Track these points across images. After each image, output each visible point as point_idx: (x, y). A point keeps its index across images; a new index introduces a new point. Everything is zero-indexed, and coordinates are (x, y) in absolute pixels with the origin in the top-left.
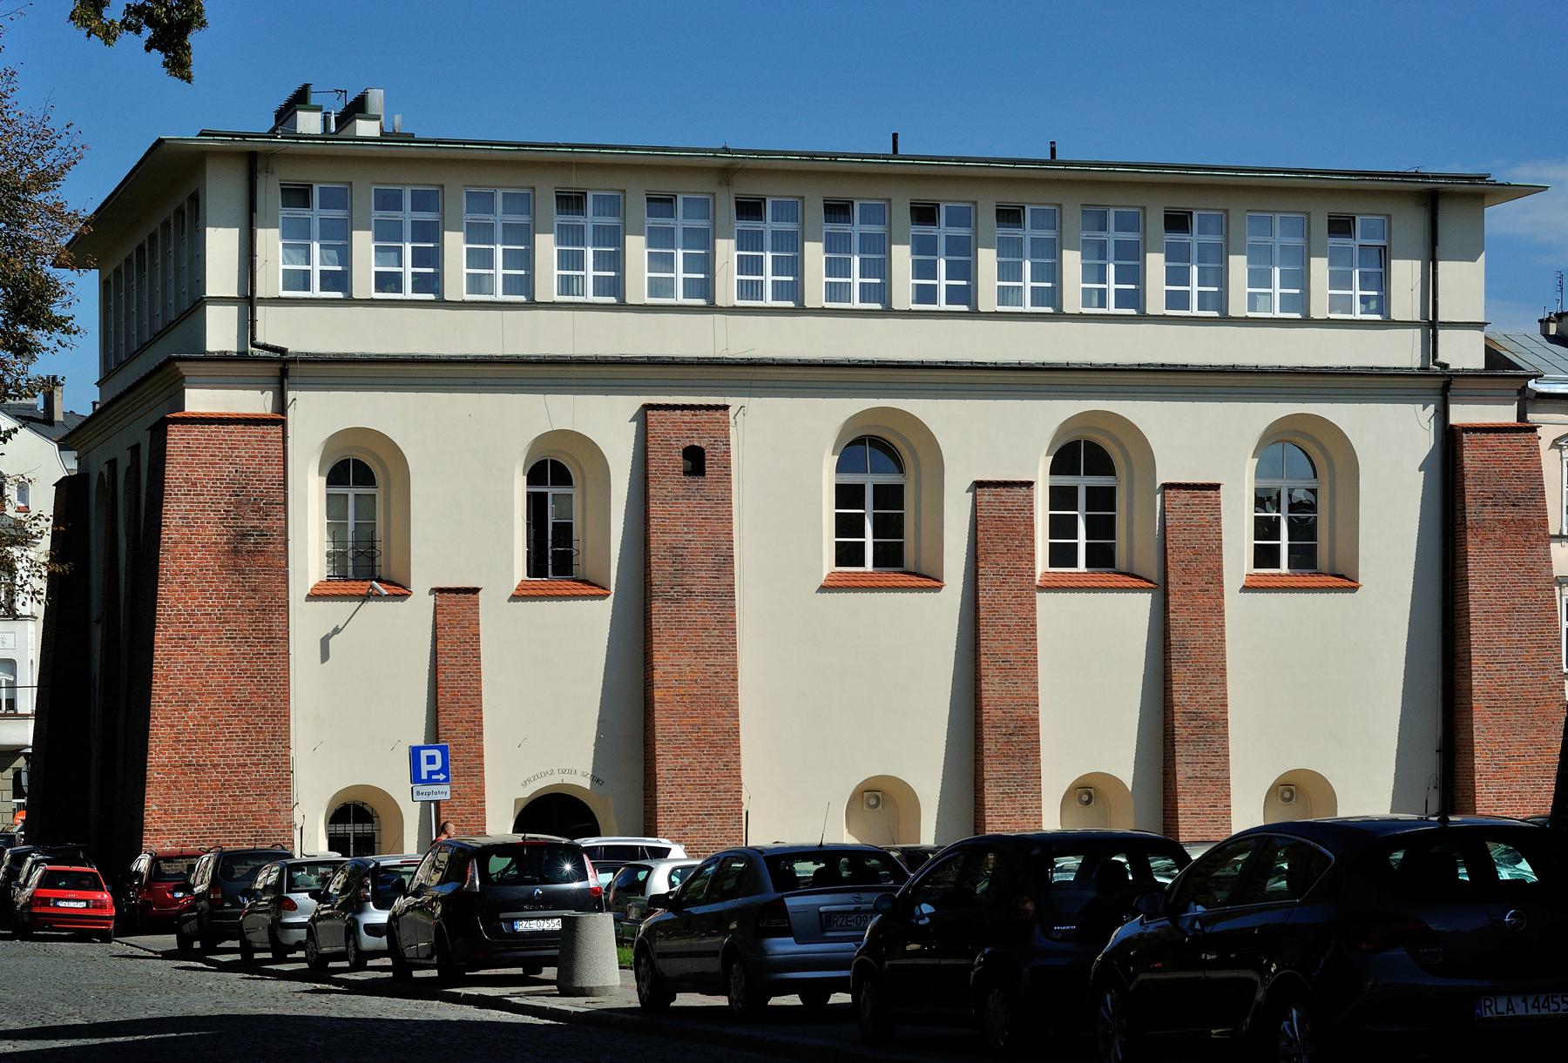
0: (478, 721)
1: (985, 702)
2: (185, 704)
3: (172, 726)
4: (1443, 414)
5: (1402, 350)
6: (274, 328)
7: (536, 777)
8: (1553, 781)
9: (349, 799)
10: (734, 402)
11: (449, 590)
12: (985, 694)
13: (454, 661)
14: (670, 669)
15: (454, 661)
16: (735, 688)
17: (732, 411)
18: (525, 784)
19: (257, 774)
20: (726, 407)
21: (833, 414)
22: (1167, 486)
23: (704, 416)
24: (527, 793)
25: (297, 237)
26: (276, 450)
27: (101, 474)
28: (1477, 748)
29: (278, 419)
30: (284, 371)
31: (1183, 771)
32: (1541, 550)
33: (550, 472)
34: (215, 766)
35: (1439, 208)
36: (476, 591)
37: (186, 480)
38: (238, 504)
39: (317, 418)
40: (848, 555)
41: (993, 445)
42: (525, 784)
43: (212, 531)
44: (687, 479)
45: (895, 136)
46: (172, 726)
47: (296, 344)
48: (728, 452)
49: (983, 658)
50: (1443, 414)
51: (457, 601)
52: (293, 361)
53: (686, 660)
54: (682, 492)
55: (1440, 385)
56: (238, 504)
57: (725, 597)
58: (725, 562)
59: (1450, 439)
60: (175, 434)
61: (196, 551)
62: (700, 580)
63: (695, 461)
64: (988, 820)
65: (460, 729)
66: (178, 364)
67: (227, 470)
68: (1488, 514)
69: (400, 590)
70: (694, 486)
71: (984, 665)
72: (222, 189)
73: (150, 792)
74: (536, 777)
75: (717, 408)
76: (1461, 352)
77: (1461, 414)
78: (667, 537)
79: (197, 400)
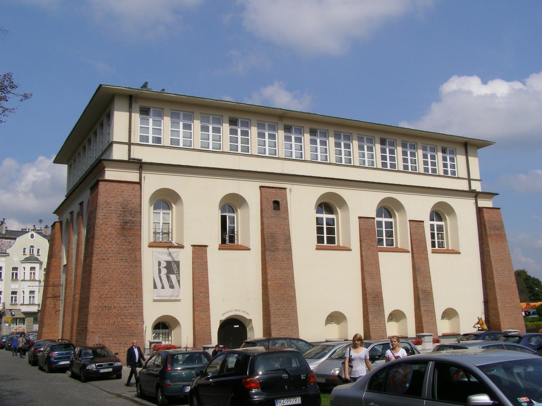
0: (207, 292)
1: (367, 287)
2: (104, 284)
3: (99, 292)
4: (476, 203)
5: (463, 185)
6: (138, 153)
8: (500, 318)
9: (161, 321)
11: (197, 246)
12: (367, 284)
13: (199, 271)
14: (272, 274)
15: (199, 271)
17: (288, 190)
18: (223, 315)
22: (410, 221)
24: (224, 318)
26: (137, 193)
27: (67, 219)
28: (498, 301)
30: (140, 165)
31: (423, 309)
32: (505, 243)
33: (231, 204)
34: (115, 307)
36: (206, 246)
37: (106, 202)
38: (124, 212)
39: (152, 183)
40: (320, 240)
41: (362, 204)
42: (223, 315)
43: (115, 221)
44: (275, 211)
45: (155, 301)
46: (99, 292)
47: (146, 159)
48: (287, 203)
49: (365, 273)
50: (476, 203)
51: (200, 251)
52: (145, 163)
54: (273, 215)
55: (476, 195)
56: (124, 212)
57: (289, 250)
58: (288, 239)
59: (480, 211)
60: (102, 185)
61: (109, 227)
63: (276, 204)
64: (371, 325)
65: (201, 295)
66: (104, 162)
67: (121, 200)
68: (492, 232)
70: (277, 213)
71: (365, 275)
73: (90, 317)
75: (283, 188)
76: (477, 186)
77: (482, 203)
78: (269, 230)
79: (110, 174)
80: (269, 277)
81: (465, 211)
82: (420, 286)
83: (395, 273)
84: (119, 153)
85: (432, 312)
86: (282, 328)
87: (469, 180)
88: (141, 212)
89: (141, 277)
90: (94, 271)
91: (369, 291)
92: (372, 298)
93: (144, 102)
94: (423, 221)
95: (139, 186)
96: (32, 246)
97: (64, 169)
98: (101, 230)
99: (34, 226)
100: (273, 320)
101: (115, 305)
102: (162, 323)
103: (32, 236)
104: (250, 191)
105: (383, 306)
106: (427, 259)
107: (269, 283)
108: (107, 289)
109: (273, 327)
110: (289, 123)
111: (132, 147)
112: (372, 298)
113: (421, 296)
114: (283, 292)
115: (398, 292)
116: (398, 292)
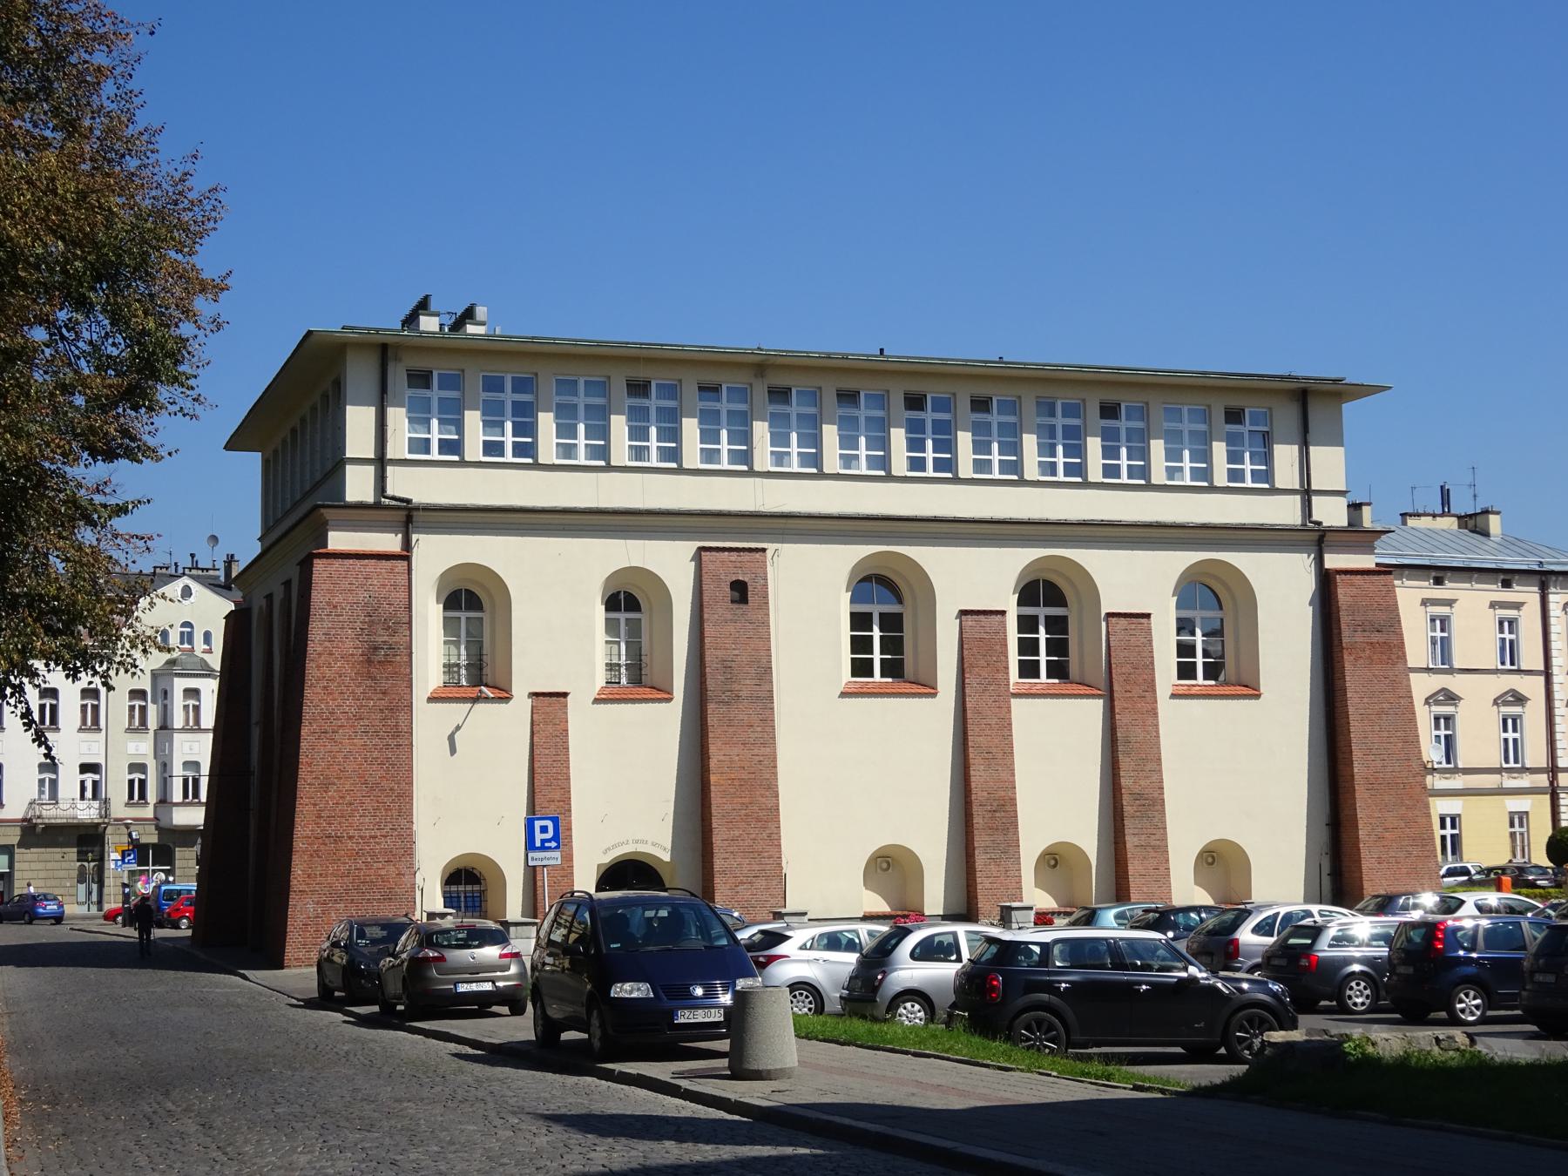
1: (973, 785)
2: (325, 787)
5: (1285, 512)
6: (402, 483)
7: (614, 846)
9: (461, 865)
10: (771, 547)
16: (775, 774)
17: (769, 554)
18: (605, 852)
19: (386, 844)
20: (764, 550)
21: (847, 557)
23: (746, 556)
24: (607, 859)
25: (419, 418)
26: (402, 579)
29: (405, 556)
31: (1131, 841)
34: (350, 838)
35: (1309, 405)
36: (565, 695)
38: (371, 623)
39: (436, 554)
40: (861, 668)
41: (973, 582)
42: (605, 852)
43: (350, 645)
47: (419, 497)
48: (766, 585)
51: (550, 702)
52: (417, 509)
53: (736, 751)
55: (1317, 539)
56: (371, 623)
58: (764, 673)
59: (1326, 581)
60: (319, 566)
61: (336, 660)
62: (746, 687)
63: (740, 591)
67: (362, 595)
68: (1359, 638)
69: (504, 696)
70: (739, 612)
72: (359, 373)
74: (614, 846)
75: (757, 550)
76: (1331, 513)
77: (1333, 561)
78: (719, 653)
79: (338, 540)
80: (713, 763)
81: (1282, 589)
82: (1126, 782)
83: (1054, 755)
84: (358, 485)
85: (1010, 847)
86: (742, 883)
87: (1307, 494)
88: (410, 623)
89: (411, 770)
90: (303, 759)
91: (978, 794)
92: (979, 811)
93: (410, 364)
94: (1148, 616)
95: (403, 564)
96: (187, 624)
97: (251, 463)
98: (318, 667)
99: (193, 556)
100: (718, 864)
101: (351, 833)
102: (467, 871)
103: (187, 592)
104: (672, 563)
105: (1016, 833)
106: (1154, 713)
107: (713, 778)
108: (332, 798)
109: (718, 880)
110: (780, 380)
111: (390, 470)
112: (979, 811)
113: (1128, 810)
114: (747, 800)
115: (1056, 800)
116: (1056, 800)
